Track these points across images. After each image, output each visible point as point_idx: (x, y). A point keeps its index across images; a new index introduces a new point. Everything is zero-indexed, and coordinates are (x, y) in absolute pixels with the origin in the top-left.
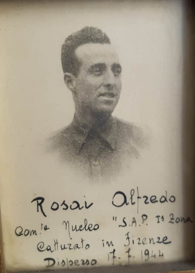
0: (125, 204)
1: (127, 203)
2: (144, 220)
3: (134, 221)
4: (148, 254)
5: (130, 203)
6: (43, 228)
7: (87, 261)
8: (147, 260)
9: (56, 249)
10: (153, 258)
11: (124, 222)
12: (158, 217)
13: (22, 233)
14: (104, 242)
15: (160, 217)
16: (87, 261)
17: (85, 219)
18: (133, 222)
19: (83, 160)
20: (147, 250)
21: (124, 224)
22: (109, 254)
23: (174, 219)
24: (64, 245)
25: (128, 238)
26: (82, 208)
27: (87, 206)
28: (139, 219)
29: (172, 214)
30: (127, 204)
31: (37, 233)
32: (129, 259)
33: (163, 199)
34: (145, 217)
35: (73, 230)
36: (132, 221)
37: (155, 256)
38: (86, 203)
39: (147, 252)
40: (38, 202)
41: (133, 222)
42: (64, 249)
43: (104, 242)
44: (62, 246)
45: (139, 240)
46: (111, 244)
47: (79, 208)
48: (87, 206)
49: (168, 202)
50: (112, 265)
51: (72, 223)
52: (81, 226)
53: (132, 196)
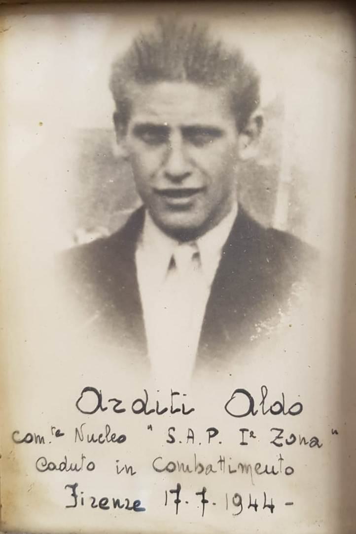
0: (100, 409)
1: (254, 411)
2: (210, 436)
3: (191, 435)
4: (240, 503)
5: (260, 413)
6: (54, 433)
12: (243, 430)
14: (118, 464)
17: (107, 426)
18: (189, 437)
19: (263, 328)
20: (91, 463)
22: (169, 493)
24: (75, 465)
25: (74, 495)
27: (265, 412)
30: (254, 414)
33: (277, 408)
35: (250, 465)
39: (237, 500)
40: (209, 433)
41: (189, 437)
42: (75, 471)
43: (118, 464)
44: (73, 465)
46: (182, 467)
47: (253, 413)
48: (265, 412)
51: (87, 432)
52: (101, 436)
53: (264, 398)
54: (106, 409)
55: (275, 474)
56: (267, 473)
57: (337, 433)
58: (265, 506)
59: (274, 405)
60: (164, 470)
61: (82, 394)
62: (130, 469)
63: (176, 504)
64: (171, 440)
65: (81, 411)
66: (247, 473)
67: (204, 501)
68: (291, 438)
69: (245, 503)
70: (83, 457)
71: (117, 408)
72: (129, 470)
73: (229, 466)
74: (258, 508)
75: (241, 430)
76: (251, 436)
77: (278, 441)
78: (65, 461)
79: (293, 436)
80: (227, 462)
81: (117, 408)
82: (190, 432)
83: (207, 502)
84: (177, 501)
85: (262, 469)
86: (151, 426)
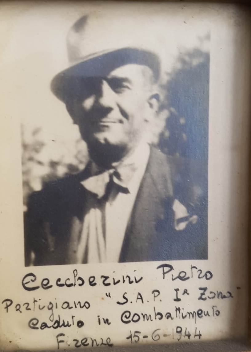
4: (180, 332)
8: (137, 342)
10: (187, 338)
11: (124, 298)
13: (37, 326)
15: (197, 268)
21: (125, 301)
26: (43, 308)
32: (58, 345)
34: (156, 293)
37: (189, 336)
38: (114, 279)
41: (138, 298)
46: (150, 318)
50: (130, 343)
57: (232, 297)
64: (41, 307)
66: (193, 318)
68: (50, 305)
70: (73, 317)
71: (106, 282)
72: (107, 321)
76: (5, 308)
77: (203, 297)
78: (58, 319)
79: (50, 303)
80: (181, 311)
81: (106, 282)
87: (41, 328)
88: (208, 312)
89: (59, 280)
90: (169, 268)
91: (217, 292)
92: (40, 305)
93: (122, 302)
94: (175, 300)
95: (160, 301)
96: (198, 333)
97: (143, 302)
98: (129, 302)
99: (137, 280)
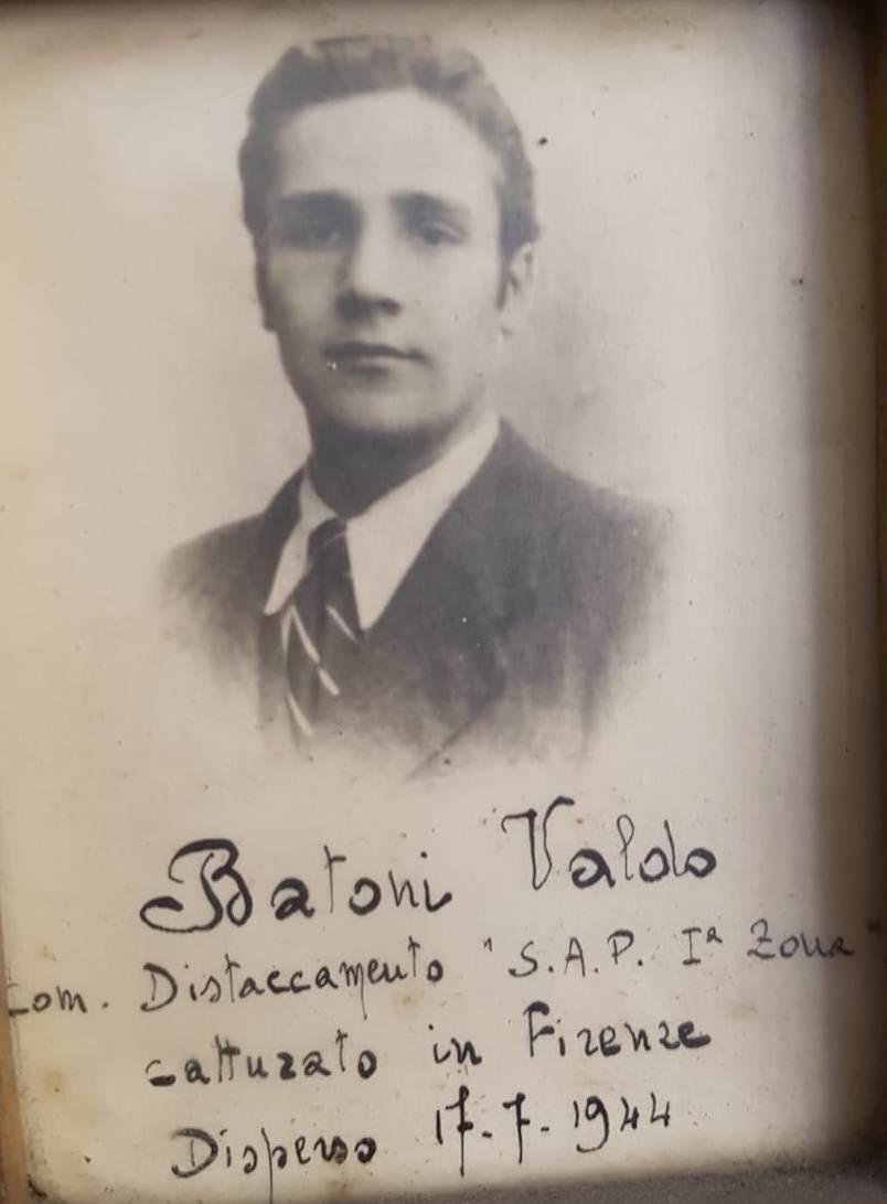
3: (575, 951)
7: (337, 1142)
9: (226, 1075)
12: (688, 932)
15: (699, 930)
16: (337, 1142)
18: (570, 958)
23: (769, 940)
27: (537, 884)
28: (597, 951)
29: (763, 921)
31: (477, 1054)
33: (655, 866)
34: (622, 942)
36: (567, 953)
41: (570, 958)
42: (258, 1077)
45: (663, 1029)
49: (340, 989)
53: (626, 845)
54: (406, 975)
55: (402, 977)
56: (390, 980)
57: (847, 953)
58: (653, 1120)
59: (647, 860)
60: (380, 979)
61: (587, 1151)
62: (67, 996)
63: (459, 1135)
65: (183, 931)
67: (521, 1122)
69: (616, 1114)
73: (627, 1026)
74: (670, 1121)
75: (684, 932)
77: (764, 948)
82: (574, 945)
83: (527, 1122)
84: (464, 1127)
85: (380, 971)
86: (489, 940)
87: (36, 1009)
88: (398, 969)
89: (275, 975)
90: (440, 1057)
91: (58, 989)
92: (251, 1055)
93: (574, 864)
94: (687, 963)
95: (546, 146)
96: (661, 1111)
97: (326, 848)
98: (542, 968)
99: (212, 983)
